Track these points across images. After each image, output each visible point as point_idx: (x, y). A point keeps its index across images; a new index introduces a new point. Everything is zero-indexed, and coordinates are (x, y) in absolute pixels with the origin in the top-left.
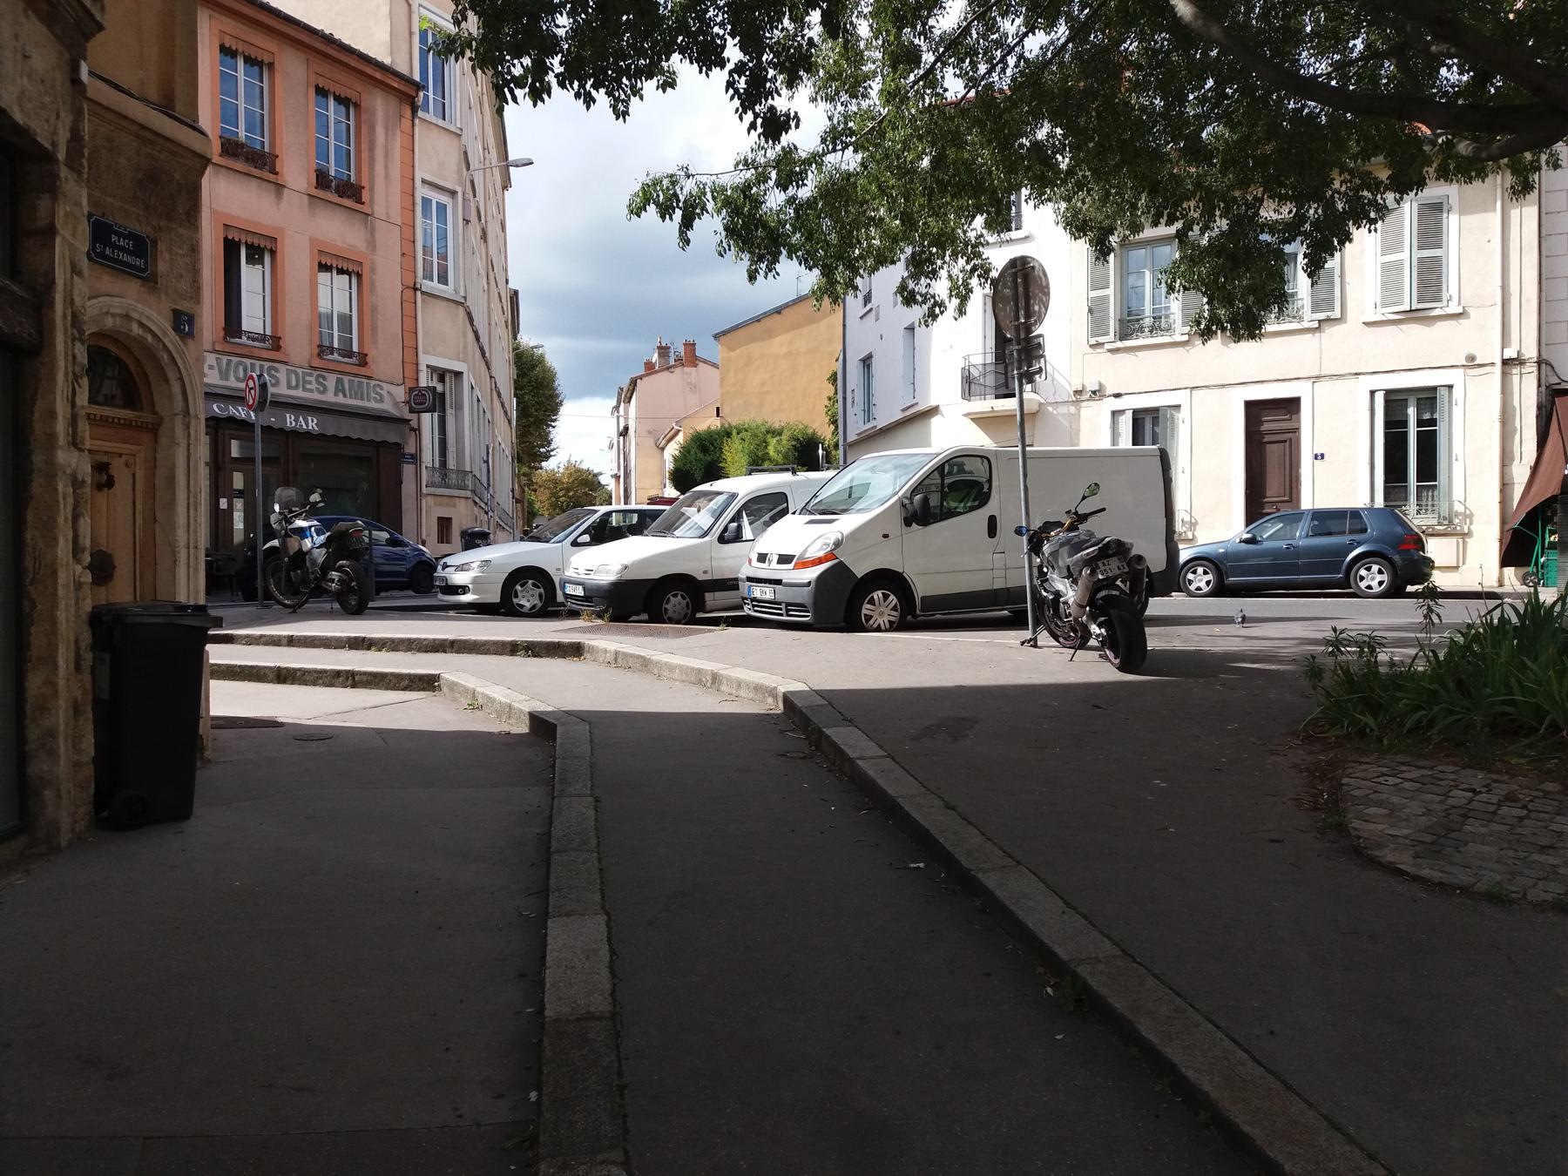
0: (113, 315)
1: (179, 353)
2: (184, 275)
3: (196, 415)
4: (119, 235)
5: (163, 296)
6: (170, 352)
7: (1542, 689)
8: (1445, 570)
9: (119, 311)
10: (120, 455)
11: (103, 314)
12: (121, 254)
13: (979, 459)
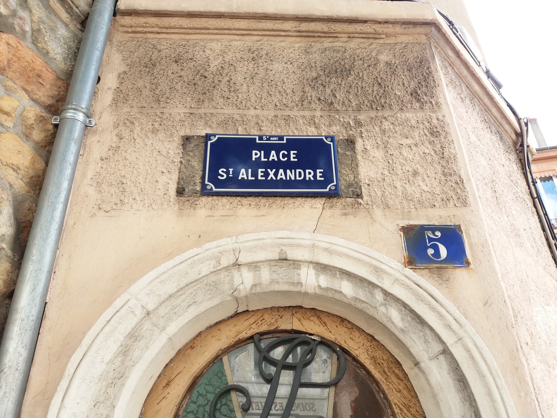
0: (254, 266)
1: (423, 300)
2: (421, 170)
4: (267, 149)
5: (378, 213)
8: (28, 373)
11: (227, 268)
12: (272, 173)
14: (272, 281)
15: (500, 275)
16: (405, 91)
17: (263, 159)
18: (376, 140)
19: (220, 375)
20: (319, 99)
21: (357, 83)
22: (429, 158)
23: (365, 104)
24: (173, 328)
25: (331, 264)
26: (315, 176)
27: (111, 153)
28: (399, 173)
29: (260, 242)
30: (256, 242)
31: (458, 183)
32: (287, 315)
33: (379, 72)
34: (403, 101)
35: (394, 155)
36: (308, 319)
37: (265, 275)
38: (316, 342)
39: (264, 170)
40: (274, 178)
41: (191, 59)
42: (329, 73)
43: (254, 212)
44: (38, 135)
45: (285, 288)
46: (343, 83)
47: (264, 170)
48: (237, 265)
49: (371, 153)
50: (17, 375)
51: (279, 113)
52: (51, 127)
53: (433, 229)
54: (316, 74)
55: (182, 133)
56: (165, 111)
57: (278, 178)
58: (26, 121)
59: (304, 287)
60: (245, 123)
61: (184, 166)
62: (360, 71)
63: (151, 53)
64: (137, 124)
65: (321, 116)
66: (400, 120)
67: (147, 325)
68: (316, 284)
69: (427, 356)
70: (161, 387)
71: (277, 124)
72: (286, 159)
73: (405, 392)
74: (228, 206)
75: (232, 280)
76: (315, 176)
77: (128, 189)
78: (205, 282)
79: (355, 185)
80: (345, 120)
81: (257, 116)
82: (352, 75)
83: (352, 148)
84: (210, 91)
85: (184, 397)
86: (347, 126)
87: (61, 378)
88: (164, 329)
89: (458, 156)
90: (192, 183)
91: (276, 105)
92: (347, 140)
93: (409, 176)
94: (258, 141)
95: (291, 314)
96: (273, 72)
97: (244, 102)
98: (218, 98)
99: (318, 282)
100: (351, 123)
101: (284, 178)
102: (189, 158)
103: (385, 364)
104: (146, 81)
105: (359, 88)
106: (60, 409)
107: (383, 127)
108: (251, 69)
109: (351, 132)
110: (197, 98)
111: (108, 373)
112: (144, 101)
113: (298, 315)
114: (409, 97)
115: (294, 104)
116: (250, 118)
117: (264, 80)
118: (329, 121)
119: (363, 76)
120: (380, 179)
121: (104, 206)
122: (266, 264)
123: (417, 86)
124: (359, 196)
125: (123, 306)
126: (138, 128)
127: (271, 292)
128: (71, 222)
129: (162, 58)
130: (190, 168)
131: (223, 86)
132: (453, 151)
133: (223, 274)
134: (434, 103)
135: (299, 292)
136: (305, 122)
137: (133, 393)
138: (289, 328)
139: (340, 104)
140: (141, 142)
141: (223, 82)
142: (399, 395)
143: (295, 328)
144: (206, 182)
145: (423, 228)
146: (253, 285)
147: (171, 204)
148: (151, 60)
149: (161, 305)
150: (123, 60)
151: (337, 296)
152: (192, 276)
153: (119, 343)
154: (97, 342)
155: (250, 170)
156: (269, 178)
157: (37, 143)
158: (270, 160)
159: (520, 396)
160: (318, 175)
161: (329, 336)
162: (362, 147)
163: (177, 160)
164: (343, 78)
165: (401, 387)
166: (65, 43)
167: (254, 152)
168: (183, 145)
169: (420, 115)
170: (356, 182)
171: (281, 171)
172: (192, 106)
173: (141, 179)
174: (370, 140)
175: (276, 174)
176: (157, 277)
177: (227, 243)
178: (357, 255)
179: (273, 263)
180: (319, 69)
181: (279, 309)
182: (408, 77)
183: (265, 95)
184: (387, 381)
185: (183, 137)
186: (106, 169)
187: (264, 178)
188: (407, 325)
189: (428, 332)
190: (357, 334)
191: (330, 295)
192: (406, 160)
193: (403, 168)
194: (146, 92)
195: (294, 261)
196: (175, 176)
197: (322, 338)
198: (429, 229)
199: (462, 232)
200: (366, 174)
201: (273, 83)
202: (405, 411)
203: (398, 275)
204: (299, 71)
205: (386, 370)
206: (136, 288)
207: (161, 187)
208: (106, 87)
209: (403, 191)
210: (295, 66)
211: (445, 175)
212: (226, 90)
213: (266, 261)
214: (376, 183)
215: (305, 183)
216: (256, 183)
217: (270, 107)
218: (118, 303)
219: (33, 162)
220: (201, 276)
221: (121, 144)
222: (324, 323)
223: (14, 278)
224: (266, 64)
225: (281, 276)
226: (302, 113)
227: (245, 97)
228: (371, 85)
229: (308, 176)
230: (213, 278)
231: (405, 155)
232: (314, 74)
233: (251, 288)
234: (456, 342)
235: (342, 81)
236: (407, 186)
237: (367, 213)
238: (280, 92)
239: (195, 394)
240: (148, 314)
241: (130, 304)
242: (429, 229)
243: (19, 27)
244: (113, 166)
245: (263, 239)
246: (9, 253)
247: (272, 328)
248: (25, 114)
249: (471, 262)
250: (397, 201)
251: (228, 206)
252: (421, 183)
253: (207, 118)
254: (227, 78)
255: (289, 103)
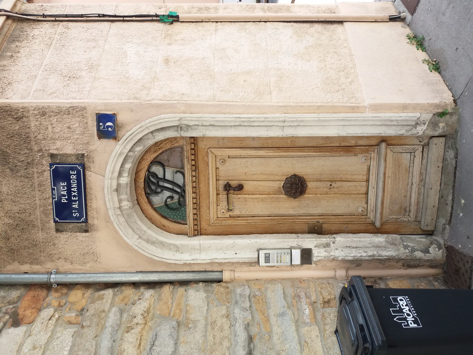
0: (120, 201)
2: (67, 125)
3: (179, 120)
6: (135, 144)
7: (29, 184)
9: (116, 199)
10: (217, 168)
11: (121, 211)
12: (74, 194)
13: (257, 257)
14: (126, 194)
15: (120, 101)
16: (16, 124)
17: (67, 197)
18: (50, 143)
19: (161, 208)
20: (26, 169)
21: (12, 148)
22: (59, 120)
23: (27, 146)
24: (145, 228)
25: (118, 171)
26: (74, 175)
27: (68, 261)
28: (69, 135)
29: (110, 200)
30: (110, 202)
31: (73, 109)
32: (138, 184)
33: (3, 135)
34: (23, 126)
35: (59, 136)
36: (139, 176)
37: (123, 197)
38: (149, 173)
39: (72, 197)
40: (77, 193)
41: (5, 232)
42: (6, 162)
43: (94, 201)
44: (65, 291)
45: (129, 189)
46: (13, 156)
47: (72, 197)
48: (120, 208)
49: (58, 147)
50: (161, 275)
51: (37, 189)
52: (59, 287)
53: (98, 126)
54: (7, 169)
55: (55, 233)
56: (41, 241)
57: (77, 191)
58: (60, 296)
59: (128, 182)
60: (45, 205)
61: (72, 230)
62: (2, 146)
63: (4, 252)
64: (51, 252)
65: (37, 168)
66: (36, 130)
67: (144, 237)
68: (127, 177)
69: (153, 140)
70: (165, 228)
71: (44, 190)
72: (65, 187)
73: (166, 142)
74: (92, 212)
75: (126, 209)
76: (74, 175)
77: (87, 251)
78: (127, 219)
79: (77, 156)
80: (39, 157)
81: (39, 199)
82: (7, 150)
83: (56, 155)
84: (26, 222)
85: (169, 220)
86: (42, 157)
87: (162, 262)
88: (145, 231)
89: (57, 105)
90: (82, 227)
91: (32, 190)
92: (51, 157)
93: (71, 131)
94: (56, 200)
95: (137, 183)
96: (9, 191)
97: (32, 206)
98: (30, 218)
99: (126, 177)
100: (40, 154)
101: (76, 188)
102: (68, 229)
103: (156, 148)
104: (23, 252)
105: (15, 148)
106: (171, 260)
107: (42, 139)
108: (8, 203)
109: (46, 155)
110: (31, 228)
111: (160, 247)
112: (37, 251)
113: (138, 180)
114: (20, 123)
115: (30, 182)
116: (42, 203)
117: (15, 196)
118: (39, 165)
119: (6, 145)
120: (73, 145)
121: (95, 260)
122: (119, 196)
123: (11, 117)
124: (83, 155)
125: (137, 246)
126: (53, 252)
127: (130, 194)
128: (103, 270)
129: (7, 246)
130: (73, 228)
131: (23, 216)
132: (55, 108)
133: (124, 212)
134: (22, 110)
135: (130, 183)
136: (41, 177)
137: (167, 238)
138: (143, 183)
139: (28, 158)
140: (61, 250)
141: (20, 216)
142: (167, 144)
143: (143, 181)
144: (81, 221)
145: (98, 130)
146: (128, 201)
147: (92, 234)
148: (9, 251)
149: (136, 234)
150: (11, 264)
151: (131, 169)
152: (126, 224)
153: (150, 245)
154: (150, 253)
155: (73, 203)
156: (77, 195)
157: (68, 290)
158: (66, 194)
159: (167, 108)
160: (73, 173)
161: (146, 168)
162: (55, 150)
163: (70, 234)
164: (9, 156)
165: (165, 143)
166: (8, 291)
167: (62, 201)
168: (61, 232)
169: (32, 118)
170: (76, 156)
171: (72, 189)
172: (37, 229)
173: (81, 247)
174: (50, 146)
175: (75, 192)
176: (126, 236)
177: (111, 213)
178: (114, 162)
179: (119, 194)
180: (4, 168)
181: (136, 187)
182: (4, 121)
183: (26, 196)
184: (162, 148)
185: (56, 232)
186: (77, 261)
187: (77, 197)
188: (142, 145)
189: (144, 137)
190: (145, 157)
191: (131, 172)
192: (62, 131)
193: (66, 133)
194: (31, 251)
195: (117, 186)
196: (79, 234)
197: (147, 171)
198: (99, 128)
199: (99, 113)
200: (71, 151)
201: (17, 192)
202: (173, 143)
203: (122, 147)
204: (7, 178)
205: (159, 148)
206: (130, 243)
207: (85, 239)
208: (30, 269)
209: (79, 135)
210: (3, 180)
211: (69, 114)
212: (25, 214)
213: (118, 197)
214: (76, 147)
215: (78, 179)
216: (80, 200)
217: (33, 193)
218: (136, 248)
219: (78, 289)
220: (125, 221)
221: (63, 257)
222: (141, 169)
223: (128, 284)
224: (3, 195)
225: (124, 191)
226: (36, 178)
227: (28, 205)
228: (13, 141)
229: (74, 178)
230: (125, 216)
231: (58, 131)
232: (8, 170)
233: (129, 202)
234: (148, 129)
235: (12, 156)
236: (77, 133)
237: (92, 152)
238: (23, 188)
239: (167, 216)
240: (140, 237)
241: (137, 244)
242: (99, 128)
243: (12, 310)
244: (75, 259)
245: (109, 199)
246: (118, 288)
247: (143, 190)
248: (57, 297)
249: (114, 112)
250: (85, 138)
251: (92, 212)
252: (75, 126)
253: (44, 222)
254: (17, 214)
255: (29, 184)
